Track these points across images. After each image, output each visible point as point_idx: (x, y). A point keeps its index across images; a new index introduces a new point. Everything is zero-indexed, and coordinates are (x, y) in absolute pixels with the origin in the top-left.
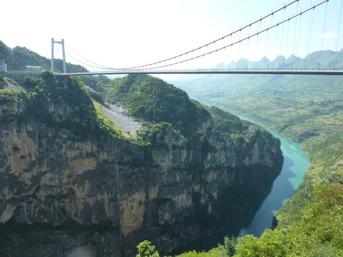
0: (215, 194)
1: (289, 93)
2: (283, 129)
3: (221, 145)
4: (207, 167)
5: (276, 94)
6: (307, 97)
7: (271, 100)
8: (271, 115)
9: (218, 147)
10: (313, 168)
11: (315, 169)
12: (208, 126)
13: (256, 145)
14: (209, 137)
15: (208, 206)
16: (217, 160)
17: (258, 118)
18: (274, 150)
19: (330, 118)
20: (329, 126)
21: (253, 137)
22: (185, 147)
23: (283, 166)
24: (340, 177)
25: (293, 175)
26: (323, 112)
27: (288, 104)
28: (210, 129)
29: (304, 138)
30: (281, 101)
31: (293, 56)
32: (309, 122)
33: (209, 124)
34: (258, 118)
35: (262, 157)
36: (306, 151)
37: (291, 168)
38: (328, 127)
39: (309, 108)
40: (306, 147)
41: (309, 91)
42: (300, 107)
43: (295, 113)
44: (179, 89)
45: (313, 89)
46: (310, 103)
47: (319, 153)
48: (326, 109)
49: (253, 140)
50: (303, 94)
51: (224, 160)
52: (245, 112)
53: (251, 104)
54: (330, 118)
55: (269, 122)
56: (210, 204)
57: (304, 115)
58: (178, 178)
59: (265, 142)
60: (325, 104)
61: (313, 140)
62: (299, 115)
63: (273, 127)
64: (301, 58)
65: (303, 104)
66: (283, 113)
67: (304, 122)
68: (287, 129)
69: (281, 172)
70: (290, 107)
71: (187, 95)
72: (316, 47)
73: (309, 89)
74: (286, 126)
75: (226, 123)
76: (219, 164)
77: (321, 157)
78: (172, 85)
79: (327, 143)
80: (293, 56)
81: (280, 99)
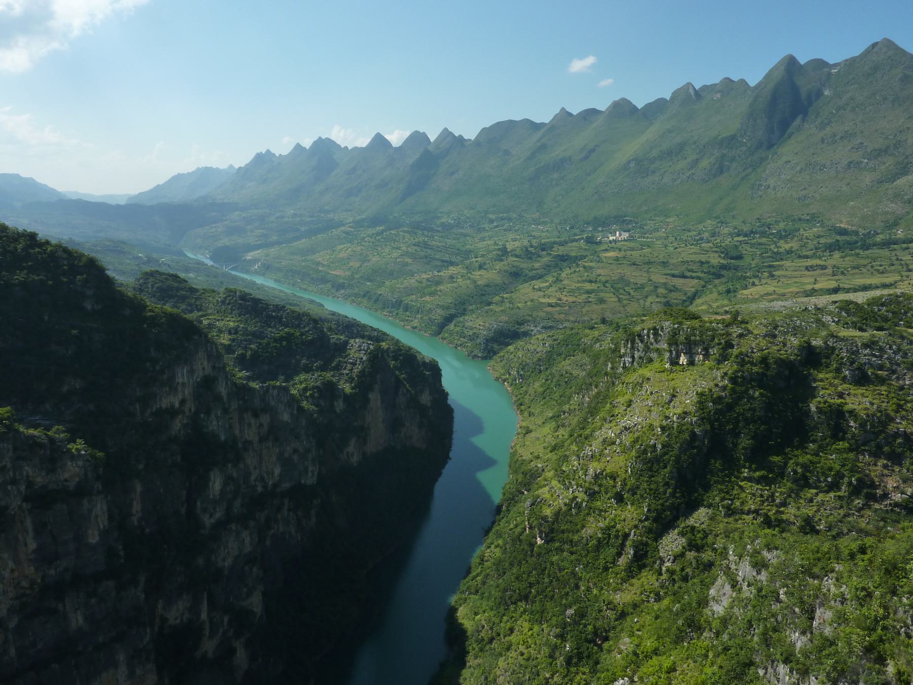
0: (255, 603)
1: (446, 228)
2: (441, 327)
3: (261, 425)
4: (208, 521)
5: (415, 233)
6: (490, 238)
7: (404, 248)
8: (409, 291)
9: (251, 435)
10: (528, 431)
11: (533, 435)
12: (199, 374)
13: (374, 397)
14: (208, 412)
15: (232, 651)
16: (253, 478)
17: (376, 301)
18: (425, 398)
19: (548, 287)
20: (549, 309)
21: (362, 373)
22: (98, 486)
23: (455, 436)
24: (615, 479)
25: (488, 462)
26: (530, 274)
27: (447, 258)
28: (208, 383)
29: (496, 346)
30: (429, 251)
31: (446, 133)
32: (502, 302)
33: (202, 366)
34: (376, 301)
35: (394, 425)
36: (504, 381)
37: (479, 441)
38: (547, 313)
39: (499, 266)
40: (502, 371)
41: (492, 221)
42: (477, 265)
43: (468, 281)
44: (65, 250)
45: (500, 215)
46: (499, 253)
47: (537, 384)
48: (537, 265)
49: (364, 383)
50: (480, 230)
51: (277, 471)
52: (340, 287)
53: (355, 264)
54: (548, 287)
55: (407, 308)
56: (239, 645)
57: (487, 286)
58: (77, 620)
59: (398, 381)
60: (533, 254)
61: (517, 351)
62: (477, 286)
63: (416, 323)
64: (466, 137)
65: (483, 256)
66: (438, 283)
67: (489, 304)
68: (451, 327)
69: (451, 454)
70: (452, 264)
71: (101, 271)
72: (188, 164)
73: (491, 216)
74: (449, 319)
75: (276, 340)
76: (260, 489)
77: (543, 395)
78: (32, 236)
79: (550, 358)
80: (446, 133)
81: (426, 245)
